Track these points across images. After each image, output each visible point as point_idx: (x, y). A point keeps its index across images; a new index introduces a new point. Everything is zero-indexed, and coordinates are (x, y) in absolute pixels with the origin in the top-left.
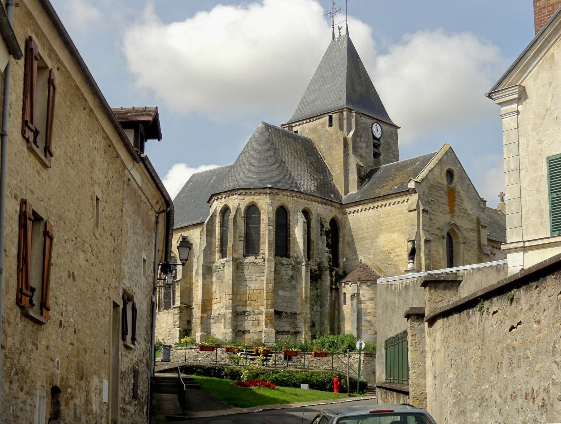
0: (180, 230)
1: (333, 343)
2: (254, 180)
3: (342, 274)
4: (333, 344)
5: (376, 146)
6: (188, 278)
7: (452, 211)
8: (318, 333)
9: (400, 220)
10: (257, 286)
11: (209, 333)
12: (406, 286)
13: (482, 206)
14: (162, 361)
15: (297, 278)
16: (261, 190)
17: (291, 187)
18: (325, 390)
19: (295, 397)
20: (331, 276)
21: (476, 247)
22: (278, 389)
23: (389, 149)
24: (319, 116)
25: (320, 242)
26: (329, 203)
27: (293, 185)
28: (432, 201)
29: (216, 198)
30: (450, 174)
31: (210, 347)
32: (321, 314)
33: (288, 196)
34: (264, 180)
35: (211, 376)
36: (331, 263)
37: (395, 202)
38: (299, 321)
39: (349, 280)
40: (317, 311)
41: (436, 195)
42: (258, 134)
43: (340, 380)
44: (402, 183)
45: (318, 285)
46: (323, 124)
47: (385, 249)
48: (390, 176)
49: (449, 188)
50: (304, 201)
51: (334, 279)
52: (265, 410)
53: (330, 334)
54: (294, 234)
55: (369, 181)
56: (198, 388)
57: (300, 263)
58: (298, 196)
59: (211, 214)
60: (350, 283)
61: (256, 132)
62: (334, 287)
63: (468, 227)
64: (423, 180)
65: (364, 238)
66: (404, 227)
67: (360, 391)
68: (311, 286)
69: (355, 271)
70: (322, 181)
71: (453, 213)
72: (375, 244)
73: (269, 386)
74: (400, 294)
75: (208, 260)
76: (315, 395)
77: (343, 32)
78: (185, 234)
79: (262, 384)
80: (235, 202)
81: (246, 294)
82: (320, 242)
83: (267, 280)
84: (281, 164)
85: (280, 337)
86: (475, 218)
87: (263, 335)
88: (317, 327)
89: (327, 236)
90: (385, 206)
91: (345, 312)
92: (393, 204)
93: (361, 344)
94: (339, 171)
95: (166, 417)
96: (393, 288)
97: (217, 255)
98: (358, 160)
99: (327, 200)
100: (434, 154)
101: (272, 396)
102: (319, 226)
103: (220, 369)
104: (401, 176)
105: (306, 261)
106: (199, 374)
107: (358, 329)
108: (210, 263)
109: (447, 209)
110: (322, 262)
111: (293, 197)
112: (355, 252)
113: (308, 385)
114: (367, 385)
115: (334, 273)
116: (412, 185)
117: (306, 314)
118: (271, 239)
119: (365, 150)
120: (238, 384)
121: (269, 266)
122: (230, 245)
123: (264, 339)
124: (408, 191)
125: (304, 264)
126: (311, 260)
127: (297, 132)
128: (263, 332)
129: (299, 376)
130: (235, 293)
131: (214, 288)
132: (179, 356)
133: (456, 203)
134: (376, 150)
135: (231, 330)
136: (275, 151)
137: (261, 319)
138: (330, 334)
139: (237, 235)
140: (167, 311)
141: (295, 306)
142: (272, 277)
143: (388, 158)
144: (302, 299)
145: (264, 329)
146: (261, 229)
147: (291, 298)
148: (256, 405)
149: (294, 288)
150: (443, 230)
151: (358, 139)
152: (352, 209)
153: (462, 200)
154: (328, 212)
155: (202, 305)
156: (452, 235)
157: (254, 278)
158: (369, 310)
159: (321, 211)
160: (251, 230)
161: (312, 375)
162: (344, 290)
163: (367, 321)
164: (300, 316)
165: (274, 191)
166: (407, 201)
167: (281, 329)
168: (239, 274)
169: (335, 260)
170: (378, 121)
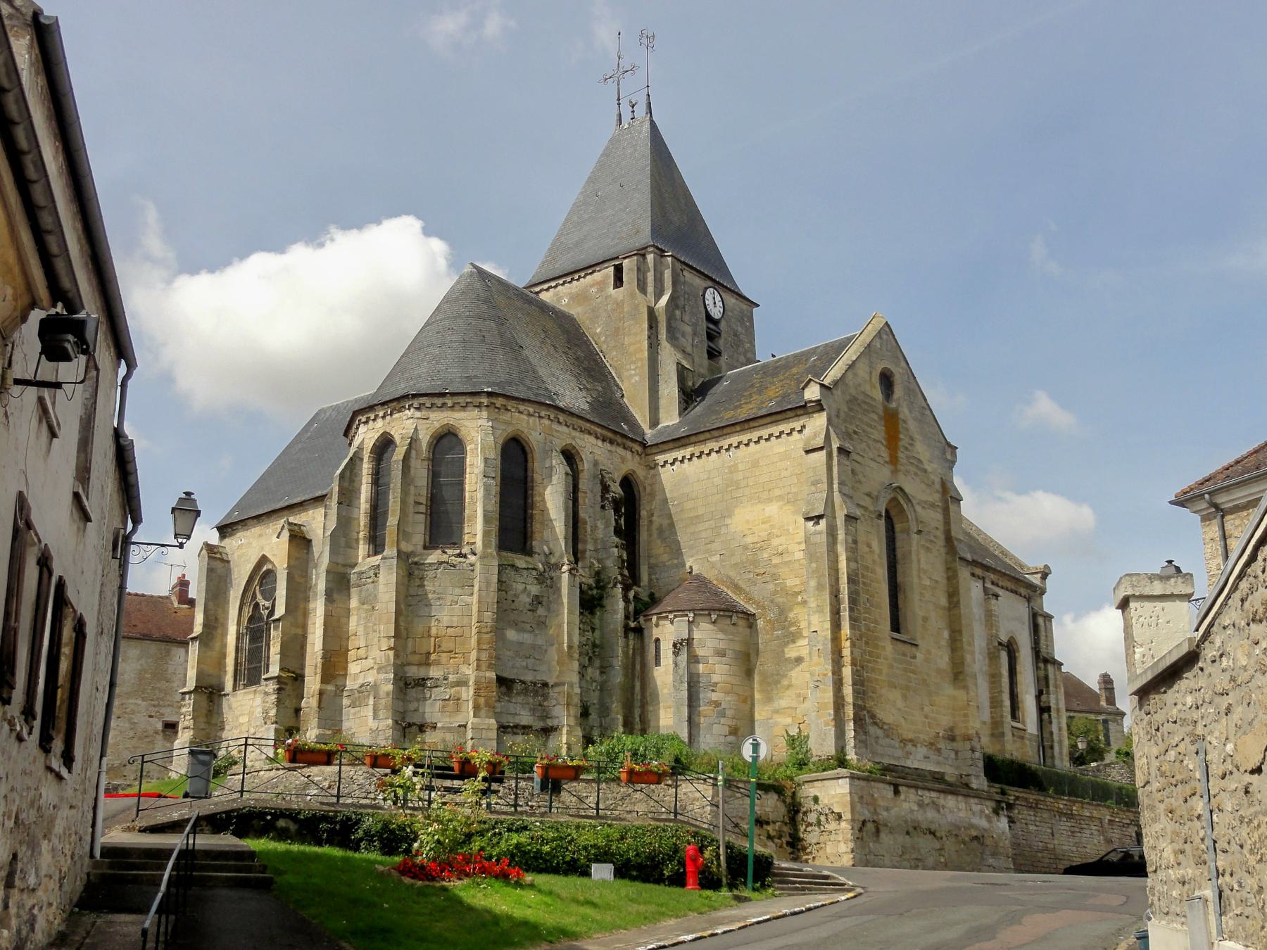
3: (646, 599)
5: (711, 336)
7: (894, 460)
9: (784, 474)
10: (455, 619)
11: (339, 731)
13: (949, 457)
16: (469, 397)
18: (659, 880)
19: (589, 911)
21: (941, 542)
22: (532, 886)
24: (591, 268)
25: (600, 525)
26: (619, 439)
28: (855, 432)
29: (364, 420)
30: (887, 380)
31: (320, 751)
32: (603, 688)
33: (529, 415)
34: (476, 377)
36: (626, 572)
38: (554, 702)
43: (701, 850)
44: (785, 396)
45: (596, 621)
46: (601, 285)
47: (749, 540)
48: (752, 386)
49: (886, 409)
50: (564, 429)
51: (632, 608)
54: (544, 500)
56: (264, 885)
57: (558, 567)
58: (552, 417)
59: (351, 455)
60: (671, 616)
62: (632, 625)
63: (924, 498)
64: (836, 383)
66: (794, 490)
67: (755, 881)
68: (581, 621)
72: (723, 530)
73: (504, 876)
75: (341, 560)
77: (641, 111)
79: (483, 870)
80: (403, 425)
81: (430, 636)
82: (600, 525)
83: (479, 602)
84: (514, 348)
85: (509, 740)
86: (937, 480)
87: (470, 734)
88: (593, 716)
89: (617, 510)
91: (659, 683)
93: (756, 747)
94: (637, 378)
97: (363, 548)
98: (679, 356)
99: (615, 432)
100: (849, 339)
101: (518, 913)
102: (598, 488)
103: (349, 819)
106: (282, 835)
107: (690, 720)
108: (344, 565)
109: (885, 454)
110: (604, 568)
111: (540, 417)
112: (677, 552)
113: (611, 867)
114: (771, 864)
115: (631, 594)
116: (812, 393)
120: (405, 870)
121: (486, 571)
122: (392, 520)
123: (470, 743)
124: (804, 406)
125: (565, 568)
128: (469, 726)
129: (586, 838)
131: (354, 623)
133: (900, 443)
135: (390, 722)
136: (501, 322)
137: (464, 696)
139: (411, 500)
140: (252, 688)
141: (544, 668)
142: (493, 596)
144: (560, 650)
146: (467, 487)
149: (542, 624)
150: (877, 497)
151: (678, 313)
152: (669, 457)
153: (912, 438)
154: (617, 460)
156: (892, 513)
157: (449, 598)
158: (715, 678)
161: (622, 838)
162: (656, 633)
163: (711, 702)
164: (557, 689)
165: (495, 399)
166: (800, 432)
167: (511, 721)
168: (413, 591)
169: (631, 565)
170: (717, 285)
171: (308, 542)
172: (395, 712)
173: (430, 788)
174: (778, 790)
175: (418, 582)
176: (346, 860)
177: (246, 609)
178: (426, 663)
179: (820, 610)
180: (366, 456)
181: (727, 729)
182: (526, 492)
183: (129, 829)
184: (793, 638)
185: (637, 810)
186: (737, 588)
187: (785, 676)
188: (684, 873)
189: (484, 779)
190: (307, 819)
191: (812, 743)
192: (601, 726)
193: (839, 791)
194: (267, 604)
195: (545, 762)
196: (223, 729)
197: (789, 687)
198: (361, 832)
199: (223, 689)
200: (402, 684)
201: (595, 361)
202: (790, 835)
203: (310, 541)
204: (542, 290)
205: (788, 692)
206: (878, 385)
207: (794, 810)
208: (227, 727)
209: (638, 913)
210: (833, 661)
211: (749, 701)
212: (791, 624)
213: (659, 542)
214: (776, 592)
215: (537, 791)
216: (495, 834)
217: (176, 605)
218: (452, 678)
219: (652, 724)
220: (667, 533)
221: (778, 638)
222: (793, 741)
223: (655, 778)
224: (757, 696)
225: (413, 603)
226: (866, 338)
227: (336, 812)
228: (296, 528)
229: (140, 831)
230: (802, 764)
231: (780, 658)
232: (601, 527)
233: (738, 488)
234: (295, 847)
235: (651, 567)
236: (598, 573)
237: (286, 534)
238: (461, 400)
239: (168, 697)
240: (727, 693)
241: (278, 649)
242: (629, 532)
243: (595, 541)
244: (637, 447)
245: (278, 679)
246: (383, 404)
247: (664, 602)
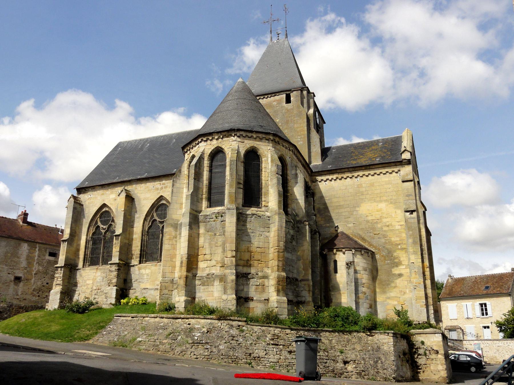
0: (120, 184)
6: (128, 233)
10: (261, 243)
11: (194, 298)
15: (297, 239)
33: (286, 148)
47: (370, 218)
60: (344, 250)
65: (340, 207)
66: (394, 198)
72: (355, 213)
78: (129, 188)
94: (302, 143)
97: (205, 203)
108: (196, 211)
124: (401, 162)
140: (95, 267)
146: (263, 178)
152: (324, 178)
164: (303, 283)
175: (242, 223)
177: (91, 228)
179: (415, 253)
180: (206, 158)
184: (398, 264)
186: (363, 239)
193: (435, 339)
197: (395, 287)
199: (77, 266)
204: (260, 99)
205: (394, 290)
214: (385, 243)
217: (21, 223)
218: (260, 274)
221: (388, 264)
231: (389, 273)
233: (362, 195)
237: (123, 195)
238: (260, 135)
239: (18, 265)
241: (118, 249)
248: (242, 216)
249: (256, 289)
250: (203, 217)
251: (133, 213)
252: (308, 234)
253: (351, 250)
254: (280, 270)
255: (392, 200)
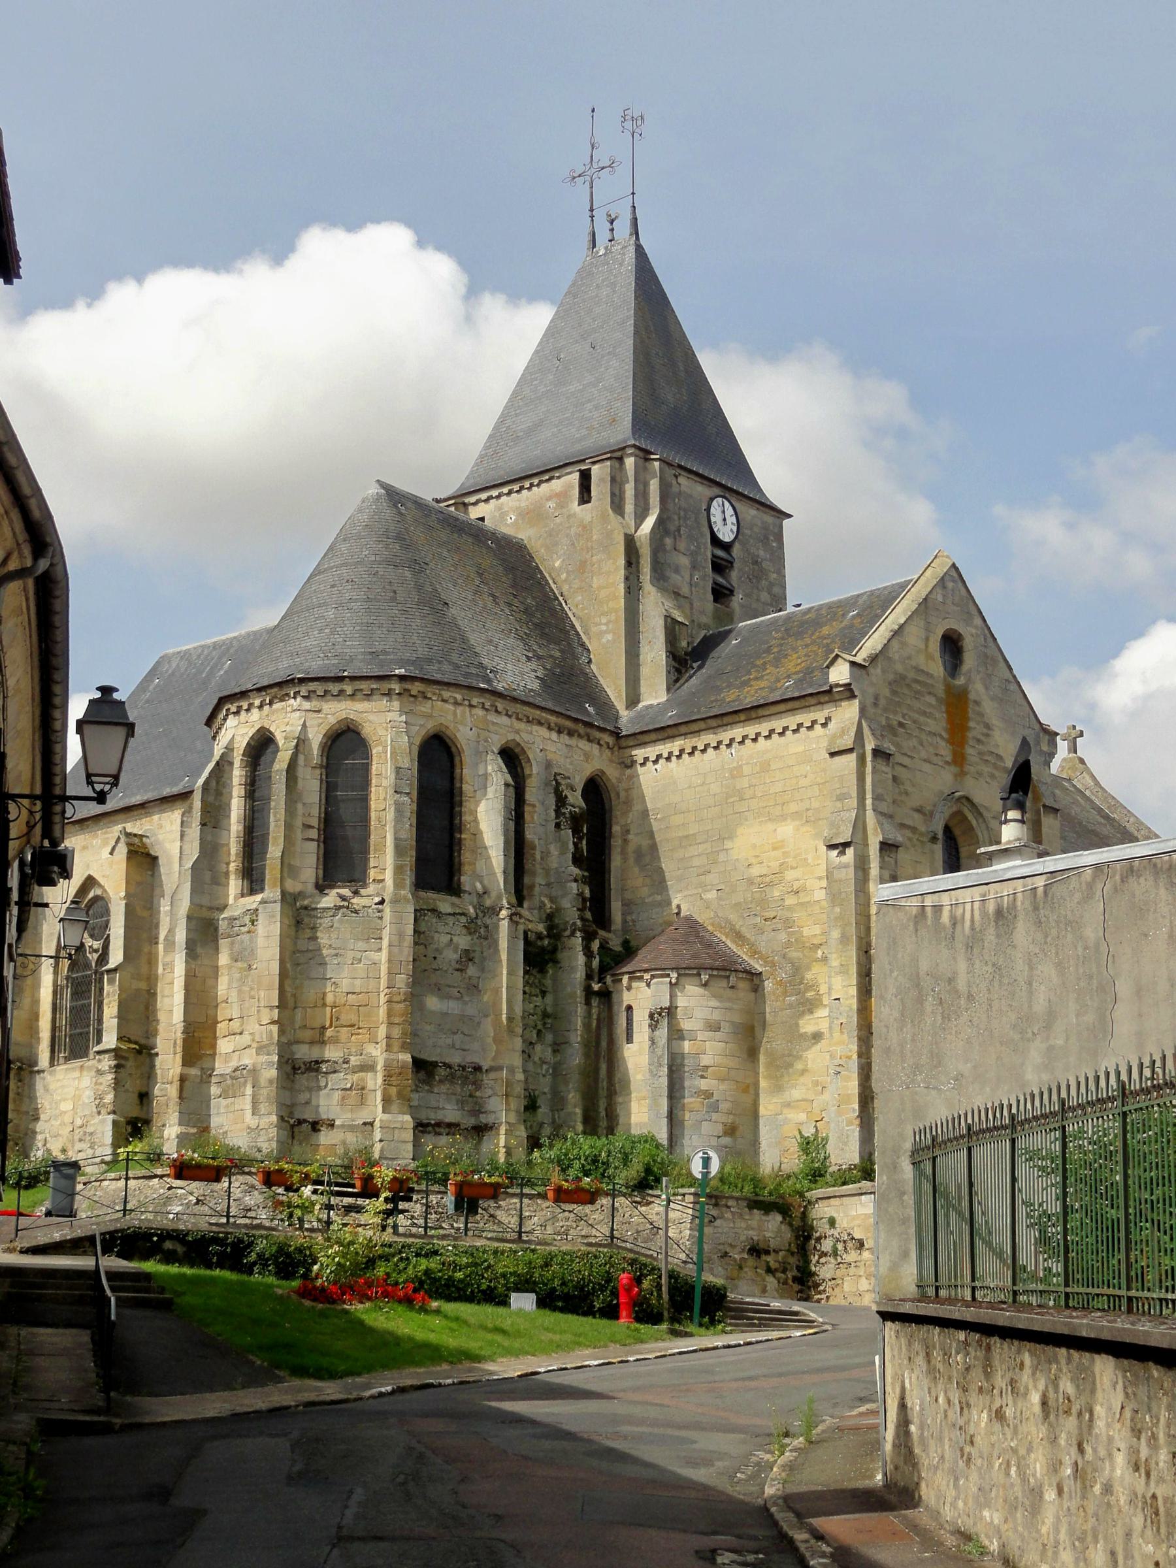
0: (121, 816)
1: (595, 1161)
2: (354, 652)
3: (619, 949)
4: (594, 1165)
5: (720, 567)
7: (959, 759)
8: (547, 1130)
9: (803, 782)
10: (358, 982)
11: (206, 1129)
12: (999, 913)
13: (1045, 748)
14: (49, 1214)
15: (484, 959)
16: (374, 683)
17: (467, 675)
18: (589, 1312)
19: (499, 1338)
20: (588, 954)
22: (437, 1312)
23: (759, 579)
24: (547, 473)
25: (554, 850)
26: (581, 729)
27: (473, 671)
28: (901, 725)
29: (233, 709)
30: (952, 645)
31: (208, 1167)
32: (557, 1071)
33: (456, 703)
34: (385, 653)
35: (209, 1266)
36: (588, 915)
37: (785, 729)
39: (645, 966)
40: (543, 1062)
41: (910, 707)
42: (364, 517)
43: (638, 1281)
44: (808, 671)
45: (548, 982)
46: (562, 497)
47: (755, 871)
48: (768, 651)
49: (949, 689)
50: (504, 720)
51: (596, 963)
52: (402, 1390)
53: (584, 1133)
54: (476, 821)
55: (700, 667)
57: (494, 911)
59: (216, 757)
60: (647, 976)
61: (360, 510)
62: (596, 987)
64: (874, 659)
66: (815, 804)
67: (702, 1316)
68: (526, 983)
69: (662, 938)
70: (559, 666)
71: (961, 766)
72: (722, 857)
73: (408, 1301)
74: (974, 941)
75: (205, 901)
76: (562, 1332)
77: (623, 229)
78: (134, 826)
79: (386, 1294)
80: (293, 721)
81: (324, 1005)
82: (554, 850)
83: (390, 961)
87: (377, 1135)
88: (543, 1110)
89: (576, 831)
90: (755, 740)
91: (630, 1065)
92: (782, 734)
94: (610, 637)
95: (40, 1421)
96: (945, 917)
97: (234, 885)
98: (669, 604)
99: (576, 720)
100: (902, 586)
101: (420, 1335)
102: (552, 801)
103: (241, 1241)
104: (802, 652)
105: (511, 905)
106: (169, 1258)
107: (671, 1116)
108: (211, 908)
109: (946, 751)
110: (558, 910)
111: (471, 706)
112: (659, 883)
113: (533, 1296)
114: (725, 1296)
115: (595, 945)
116: (840, 674)
117: (512, 1070)
118: (404, 835)
119: (687, 578)
120: (304, 1293)
121: (398, 919)
122: (274, 851)
123: (378, 1147)
124: (829, 691)
125: (504, 913)
126: (526, 905)
127: (482, 519)
128: (377, 1124)
129: (503, 1266)
130: (288, 1002)
132: (101, 1201)
133: (970, 735)
134: (720, 580)
135: (274, 1118)
136: (418, 567)
137: (370, 1084)
138: (584, 1133)
139: (298, 822)
140: (78, 1063)
141: (476, 1046)
142: (406, 952)
143: (754, 605)
145: (380, 1117)
147: (463, 1018)
148: (369, 1368)
149: (474, 988)
150: (932, 814)
151: (668, 541)
152: (651, 751)
153: (988, 726)
154: (578, 757)
155: (185, 1041)
156: (957, 832)
157: (350, 954)
158: (705, 1060)
159: (559, 755)
160: (342, 805)
161: (547, 1264)
162: (627, 998)
163: (698, 1093)
164: (492, 1075)
165: (413, 685)
166: (824, 725)
167: (433, 1117)
168: (302, 944)
169: (597, 906)
170: (728, 492)
171: (152, 861)
172: (281, 1105)
173: (329, 1207)
174: (780, 1207)
175: (308, 933)
176: (242, 1283)
178: (321, 1042)
179: (843, 969)
180: (237, 759)
181: (720, 1127)
182: (452, 808)
183: (10, 1250)
184: (810, 1006)
185: (561, 1231)
186: (739, 937)
187: (799, 1057)
188: (617, 1305)
189: (387, 1200)
190: (195, 1241)
191: (830, 1148)
192: (554, 1122)
193: (862, 1211)
194: (97, 944)
195: (459, 1178)
196: (37, 1119)
197: (804, 1072)
198: (254, 1256)
199: (36, 1063)
200: (288, 1068)
201: (553, 612)
202: (798, 1268)
203: (155, 858)
205: (802, 1080)
206: (937, 655)
207: (804, 1237)
208: (42, 1117)
209: (551, 1341)
210: (860, 1039)
211: (752, 1090)
212: (809, 988)
213: (636, 870)
214: (788, 945)
215: (451, 1210)
216: (401, 1259)
218: (354, 1061)
219: (621, 1120)
220: (647, 859)
221: (791, 1006)
222: (807, 1145)
223: (588, 1197)
224: (763, 1084)
225: (302, 960)
226: (919, 591)
227: (228, 1233)
228: (136, 840)
229: (21, 1252)
230: (816, 1175)
232: (556, 853)
233: (742, 799)
234: (187, 1271)
235: (627, 905)
236: (550, 917)
237: (122, 850)
238: (364, 685)
240: (722, 1080)
242: (594, 859)
243: (547, 872)
244: (607, 738)
245: (116, 1052)
246: (259, 690)
247: (639, 957)
248: (309, 916)
249: (343, 1098)
250: (226, 922)
251: (155, 902)
252: (503, 944)
253: (668, 975)
254: (396, 1046)
255: (810, 813)
